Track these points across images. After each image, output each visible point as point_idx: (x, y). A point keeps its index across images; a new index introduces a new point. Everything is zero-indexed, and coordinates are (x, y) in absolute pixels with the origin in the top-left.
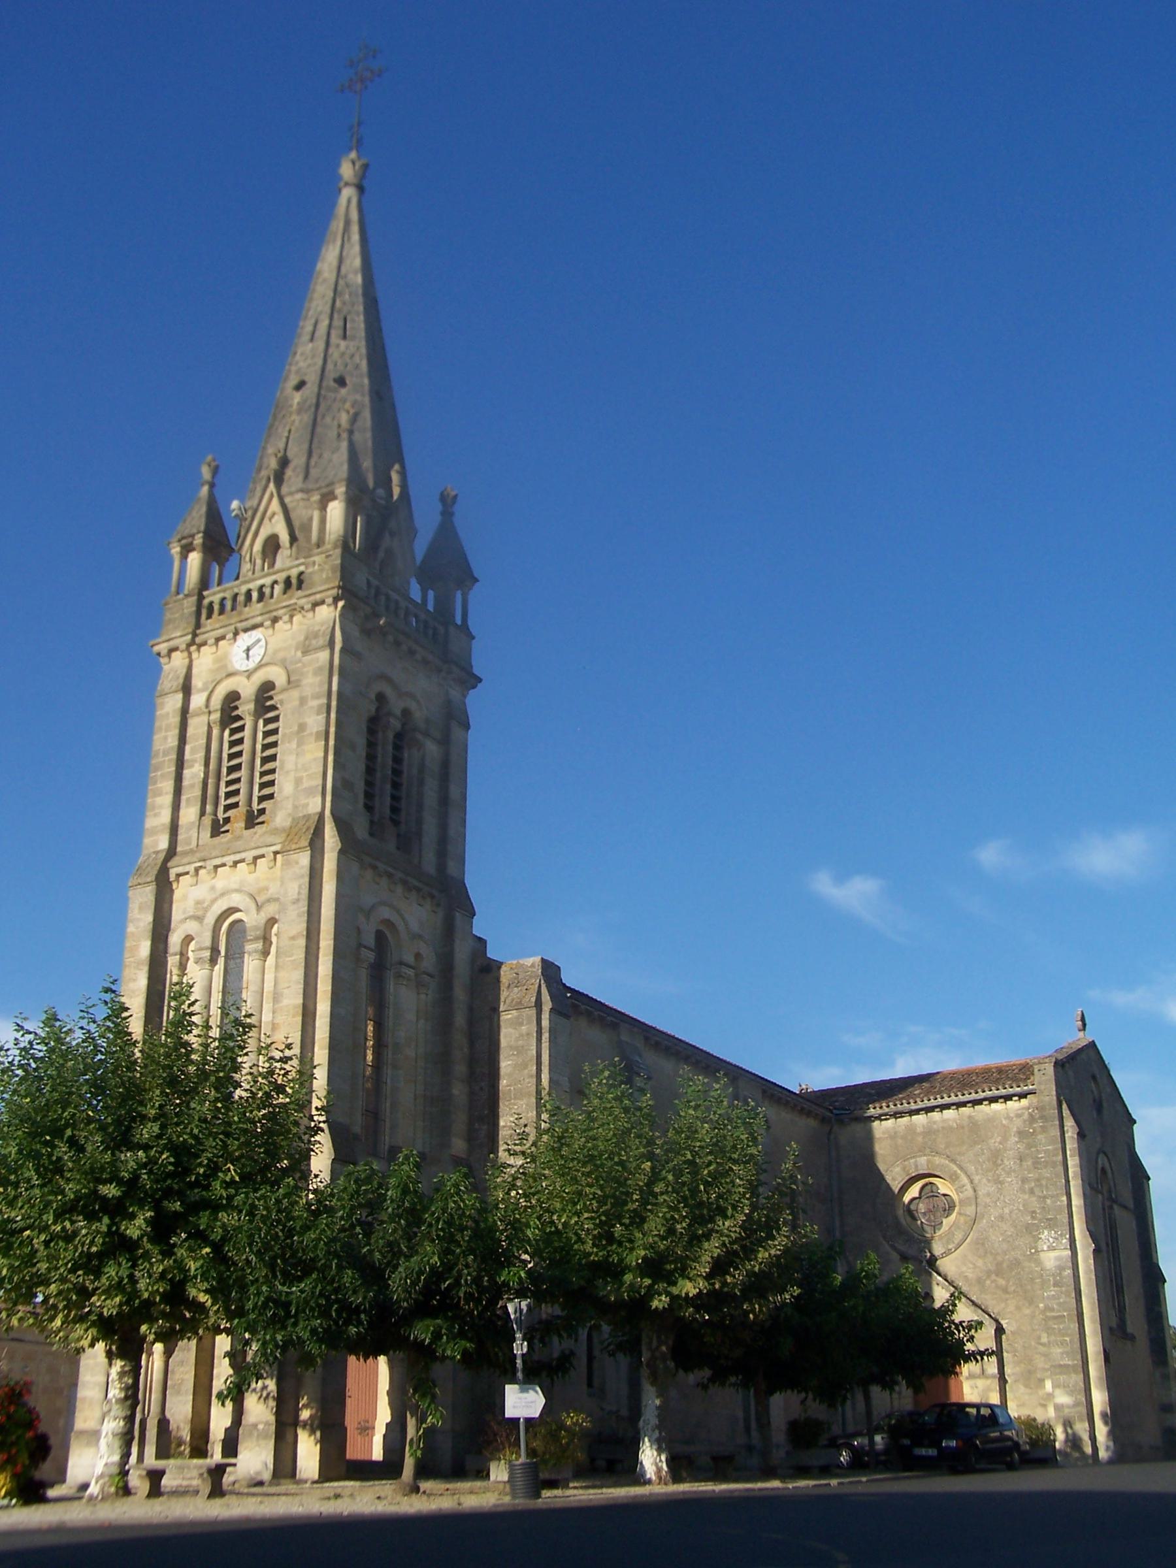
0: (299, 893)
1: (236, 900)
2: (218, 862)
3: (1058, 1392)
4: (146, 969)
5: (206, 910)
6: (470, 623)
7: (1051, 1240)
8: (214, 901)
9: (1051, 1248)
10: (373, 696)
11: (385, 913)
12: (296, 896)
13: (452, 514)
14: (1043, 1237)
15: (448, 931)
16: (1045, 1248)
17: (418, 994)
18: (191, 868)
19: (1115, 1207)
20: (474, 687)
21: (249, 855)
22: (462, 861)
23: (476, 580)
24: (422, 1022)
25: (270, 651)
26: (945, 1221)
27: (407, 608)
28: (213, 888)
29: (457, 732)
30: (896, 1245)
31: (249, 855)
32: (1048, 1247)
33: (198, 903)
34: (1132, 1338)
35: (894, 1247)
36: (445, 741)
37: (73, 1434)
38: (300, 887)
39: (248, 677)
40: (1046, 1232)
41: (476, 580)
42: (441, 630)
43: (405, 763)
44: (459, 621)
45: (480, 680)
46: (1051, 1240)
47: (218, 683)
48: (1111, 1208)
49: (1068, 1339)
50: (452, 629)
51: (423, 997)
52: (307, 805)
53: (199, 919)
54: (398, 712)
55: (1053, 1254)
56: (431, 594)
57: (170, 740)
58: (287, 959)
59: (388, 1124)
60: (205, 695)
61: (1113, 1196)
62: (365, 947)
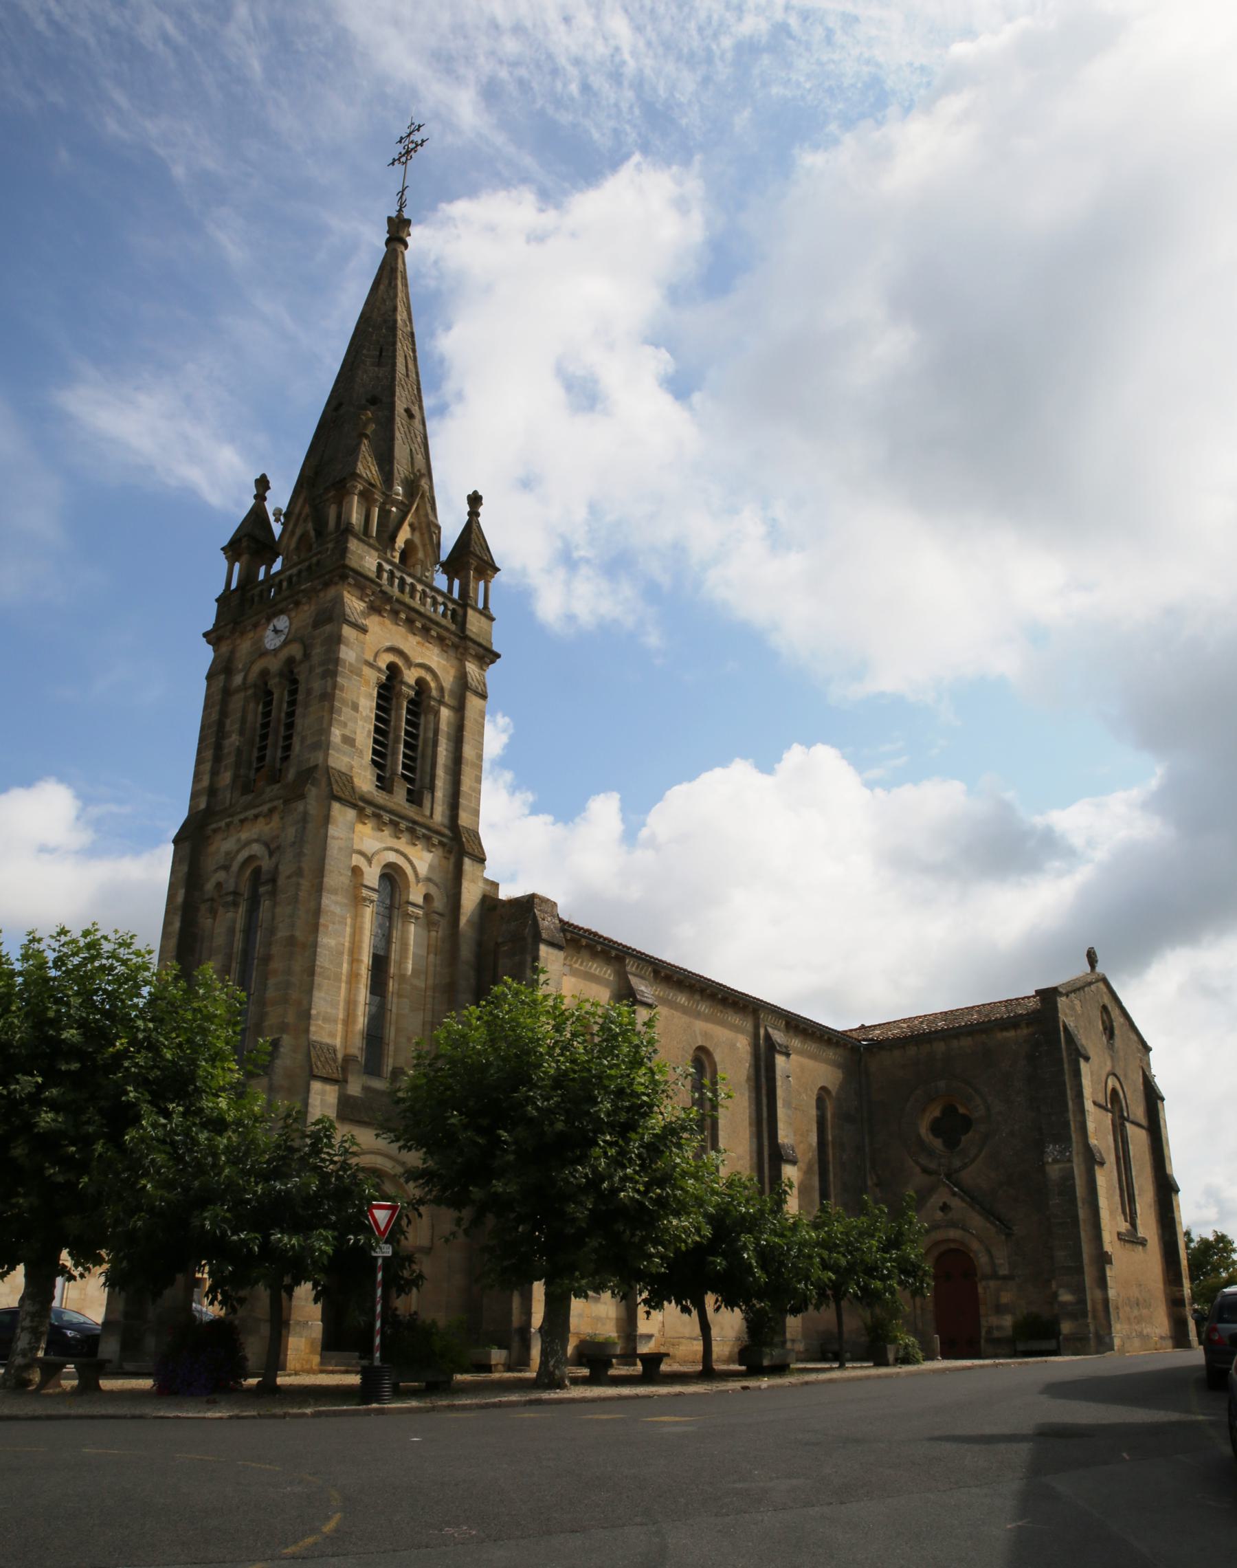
0: (296, 837)
1: (256, 849)
2: (242, 816)
3: (1061, 1291)
4: (180, 913)
5: (233, 859)
6: (490, 606)
7: (1055, 1153)
8: (238, 851)
9: (1055, 1161)
10: (384, 666)
11: (392, 857)
12: (293, 840)
13: (478, 515)
14: (1048, 1150)
15: (457, 876)
16: (1050, 1160)
17: (429, 931)
18: (222, 824)
19: (1127, 1124)
20: (493, 662)
21: (265, 808)
22: (476, 813)
23: (498, 570)
24: (432, 957)
25: (293, 631)
26: (963, 1138)
27: (424, 592)
28: (239, 840)
29: (473, 702)
30: (920, 1160)
31: (265, 808)
32: (1053, 1160)
33: (227, 853)
34: (1143, 1242)
35: (917, 1163)
36: (460, 709)
37: (570, 1335)
38: (296, 831)
39: (275, 655)
40: (1051, 1146)
41: (498, 570)
42: (460, 611)
43: (422, 728)
44: (481, 605)
45: (498, 656)
46: (1055, 1153)
47: (253, 663)
48: (1123, 1125)
49: (1071, 1243)
50: (470, 612)
51: (433, 934)
52: (310, 759)
53: (226, 868)
54: (412, 682)
55: (1057, 1167)
56: (456, 583)
57: (213, 715)
58: (283, 896)
59: (392, 1048)
60: (242, 674)
61: (1125, 1114)
62: (366, 887)
